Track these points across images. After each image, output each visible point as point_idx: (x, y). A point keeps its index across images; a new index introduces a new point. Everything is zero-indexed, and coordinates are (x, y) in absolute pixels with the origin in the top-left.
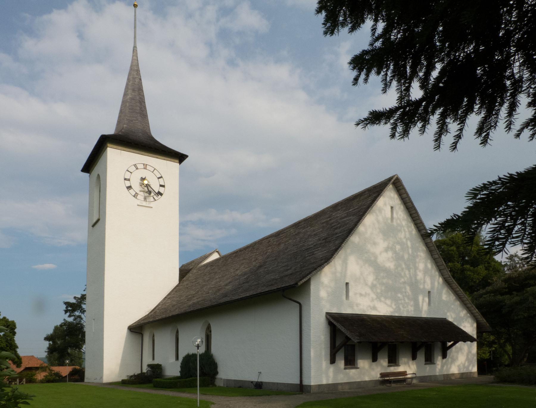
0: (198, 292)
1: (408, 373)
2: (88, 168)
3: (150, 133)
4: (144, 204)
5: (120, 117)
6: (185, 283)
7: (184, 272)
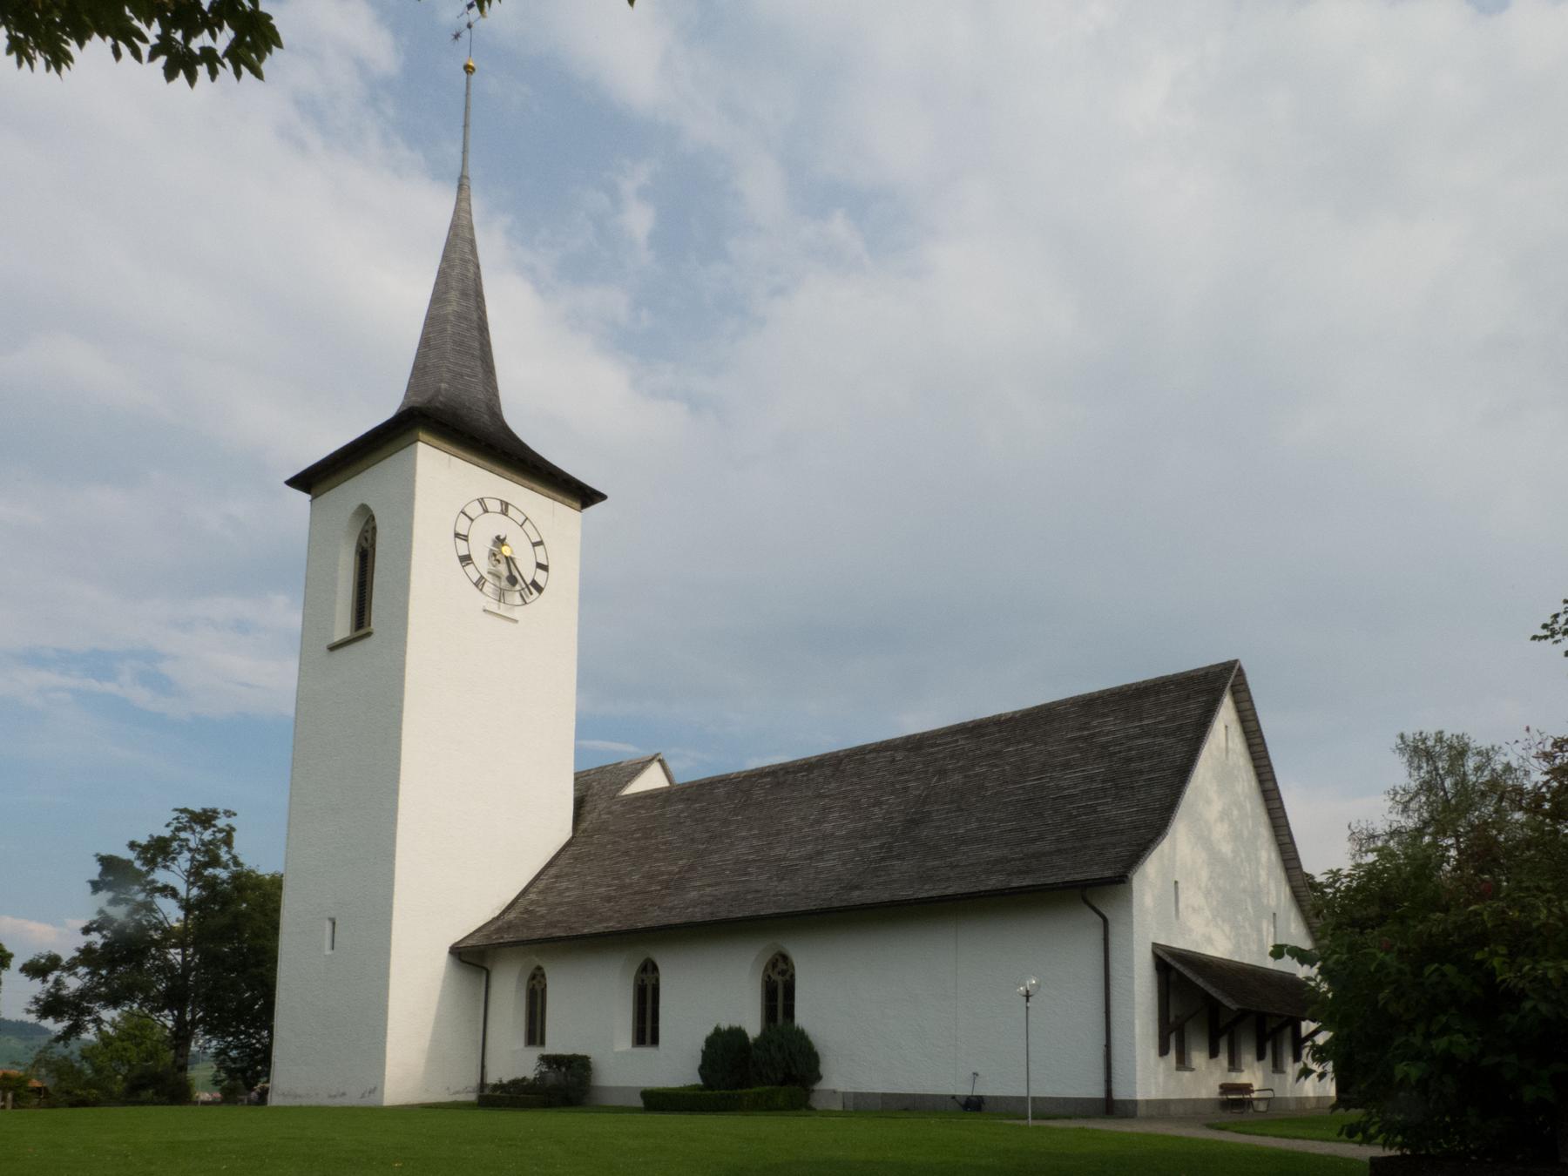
1: (1255, 1087)
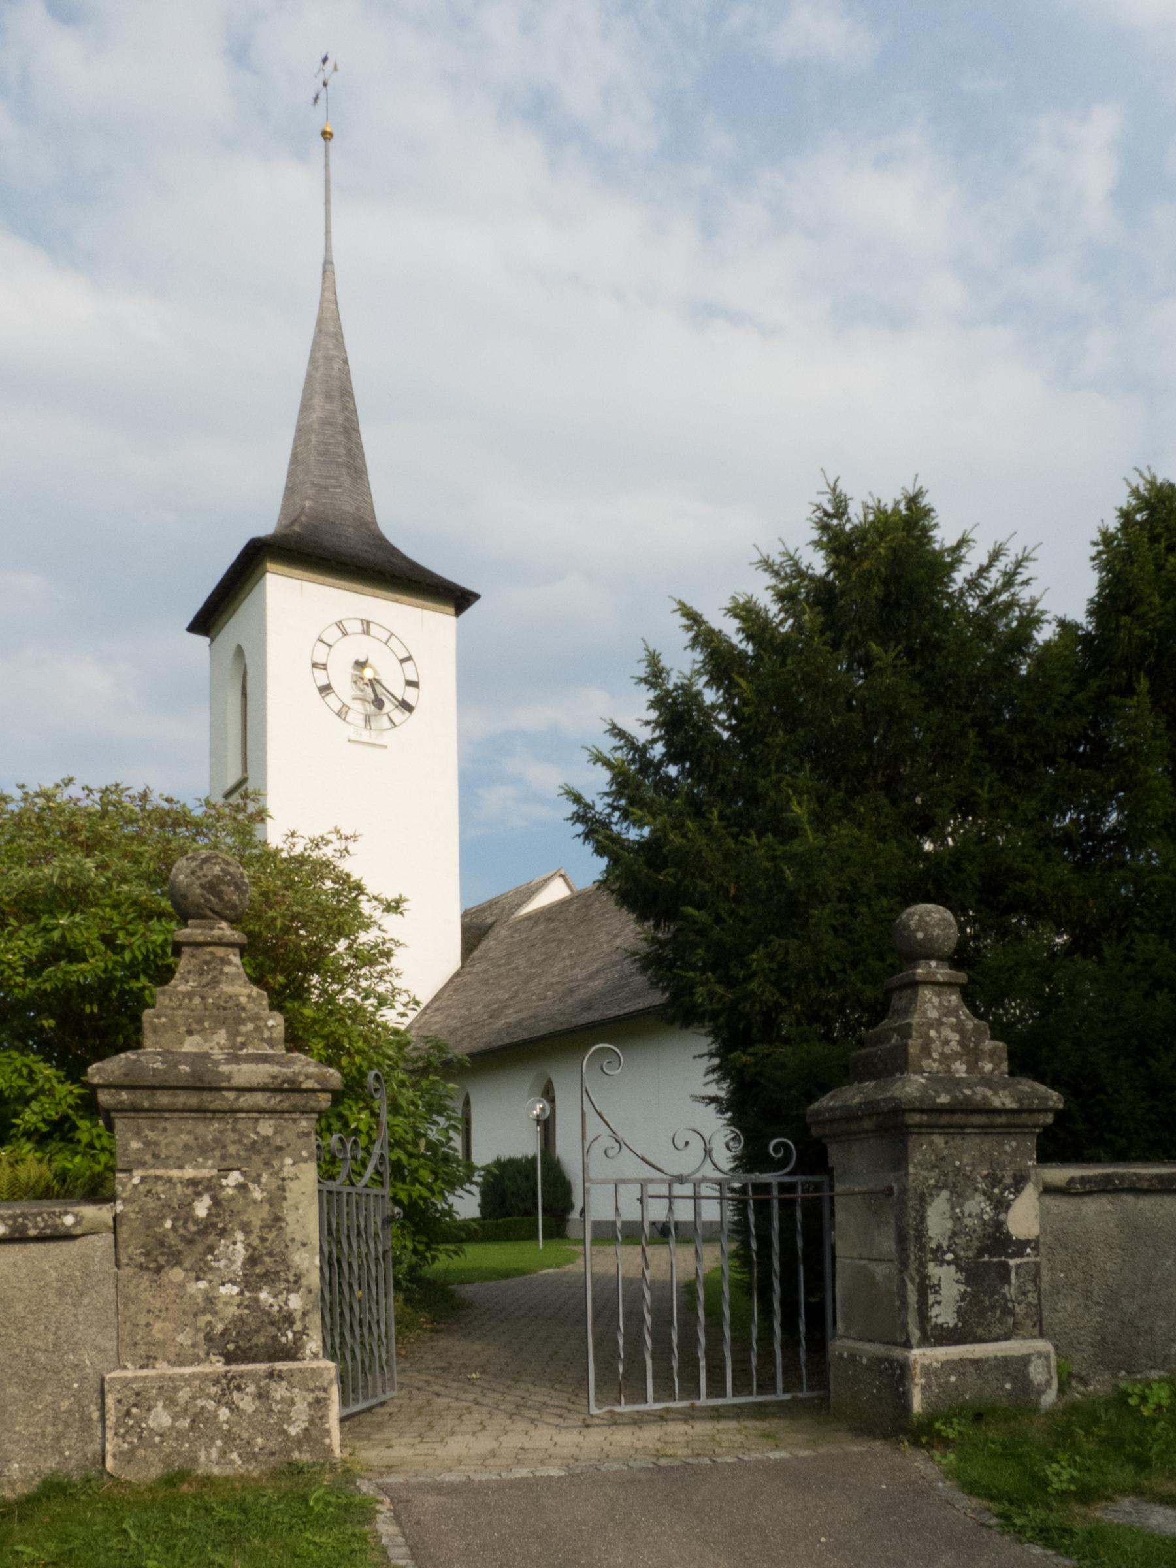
0: (516, 994)
2: (207, 622)
3: (375, 523)
4: (366, 736)
5: (291, 474)
6: (479, 967)
7: (475, 933)
